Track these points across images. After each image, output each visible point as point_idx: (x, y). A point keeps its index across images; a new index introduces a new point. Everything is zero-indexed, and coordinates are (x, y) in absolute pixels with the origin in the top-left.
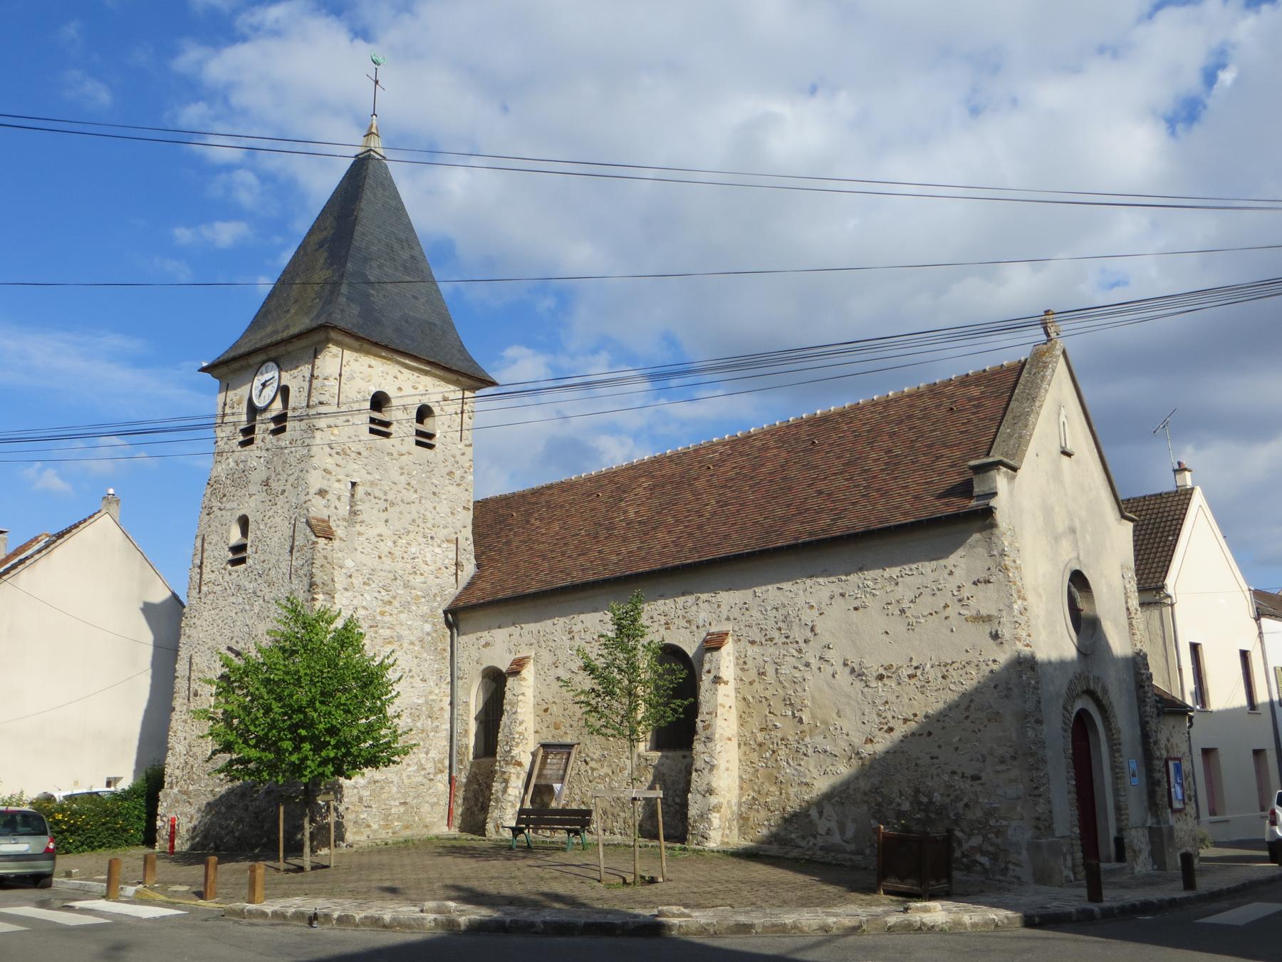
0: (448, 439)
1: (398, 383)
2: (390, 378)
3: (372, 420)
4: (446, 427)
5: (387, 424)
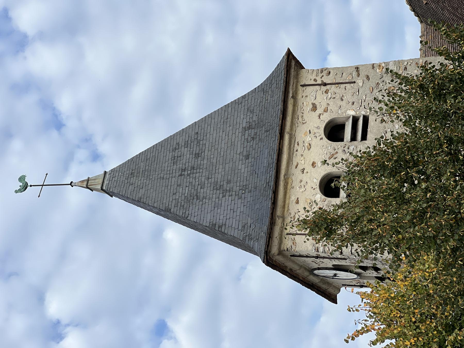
0: (355, 99)
1: (308, 168)
2: (305, 177)
3: (353, 138)
4: (343, 103)
5: (355, 120)
